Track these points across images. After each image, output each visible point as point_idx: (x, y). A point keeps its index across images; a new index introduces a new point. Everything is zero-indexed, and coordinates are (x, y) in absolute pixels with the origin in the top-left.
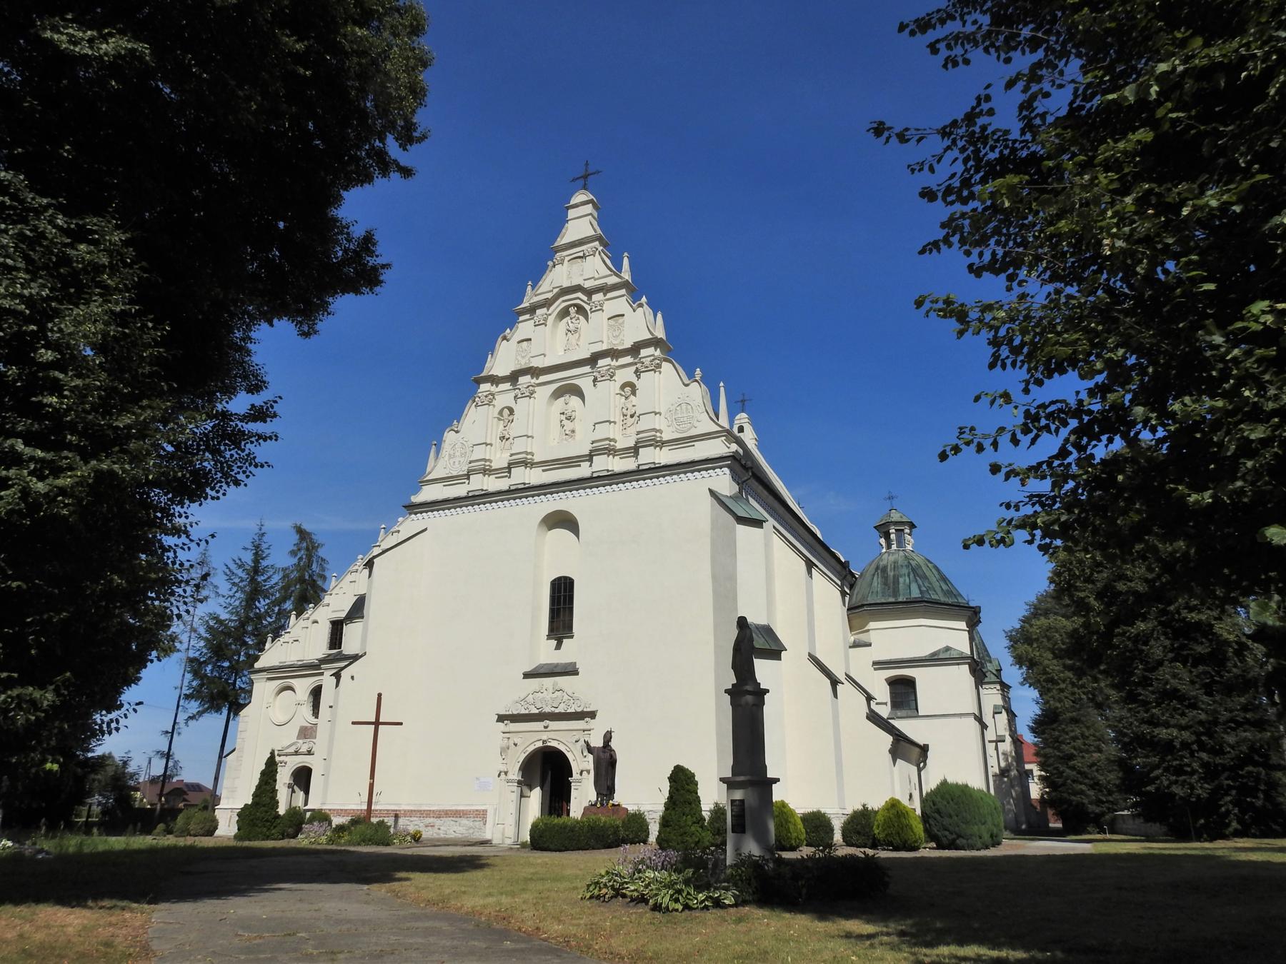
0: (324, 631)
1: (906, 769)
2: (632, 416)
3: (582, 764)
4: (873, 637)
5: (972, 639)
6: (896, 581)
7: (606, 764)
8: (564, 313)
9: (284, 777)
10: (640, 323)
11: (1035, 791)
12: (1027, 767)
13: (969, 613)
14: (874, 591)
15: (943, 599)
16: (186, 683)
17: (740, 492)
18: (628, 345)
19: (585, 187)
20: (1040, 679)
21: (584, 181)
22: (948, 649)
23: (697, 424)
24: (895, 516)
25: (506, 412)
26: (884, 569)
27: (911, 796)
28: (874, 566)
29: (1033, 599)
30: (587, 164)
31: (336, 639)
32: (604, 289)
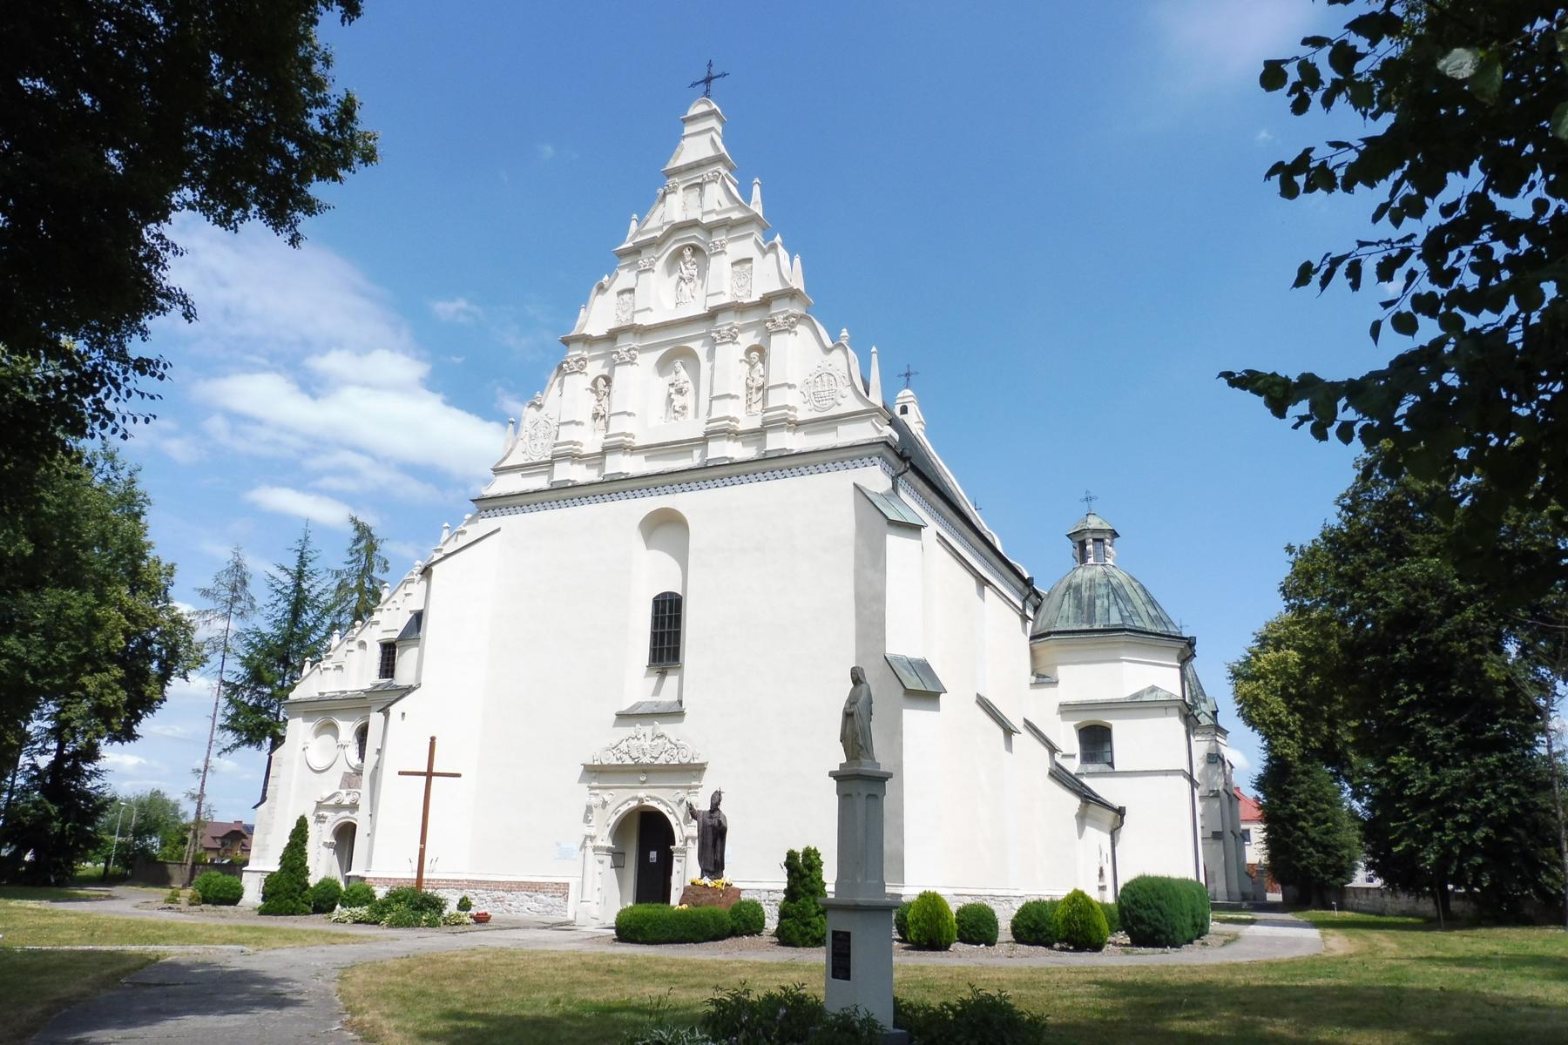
0: (375, 654)
1: (1097, 837)
2: (759, 389)
3: (685, 833)
4: (1063, 672)
5: (1183, 677)
6: (1092, 604)
7: (713, 836)
8: (678, 255)
9: (319, 839)
10: (776, 269)
11: (1255, 853)
12: (1244, 826)
13: (1182, 645)
14: (1063, 615)
15: (1150, 627)
16: (220, 711)
17: (895, 488)
18: (756, 298)
19: (707, 94)
20: (1270, 728)
22: (1153, 689)
23: (841, 401)
24: (1094, 523)
25: (602, 382)
26: (1077, 589)
27: (1101, 870)
28: (1065, 584)
29: (1260, 628)
30: (710, 65)
31: (388, 668)
32: (727, 225)
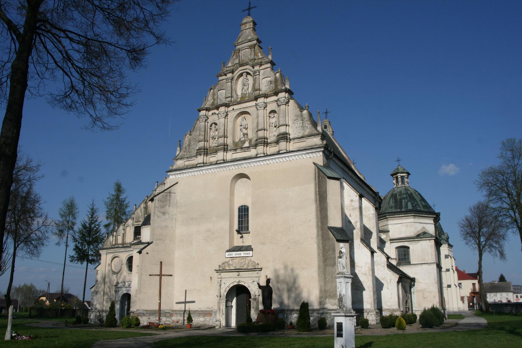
6: (401, 202)
21: (249, 11)
28: (390, 194)
30: (250, 3)
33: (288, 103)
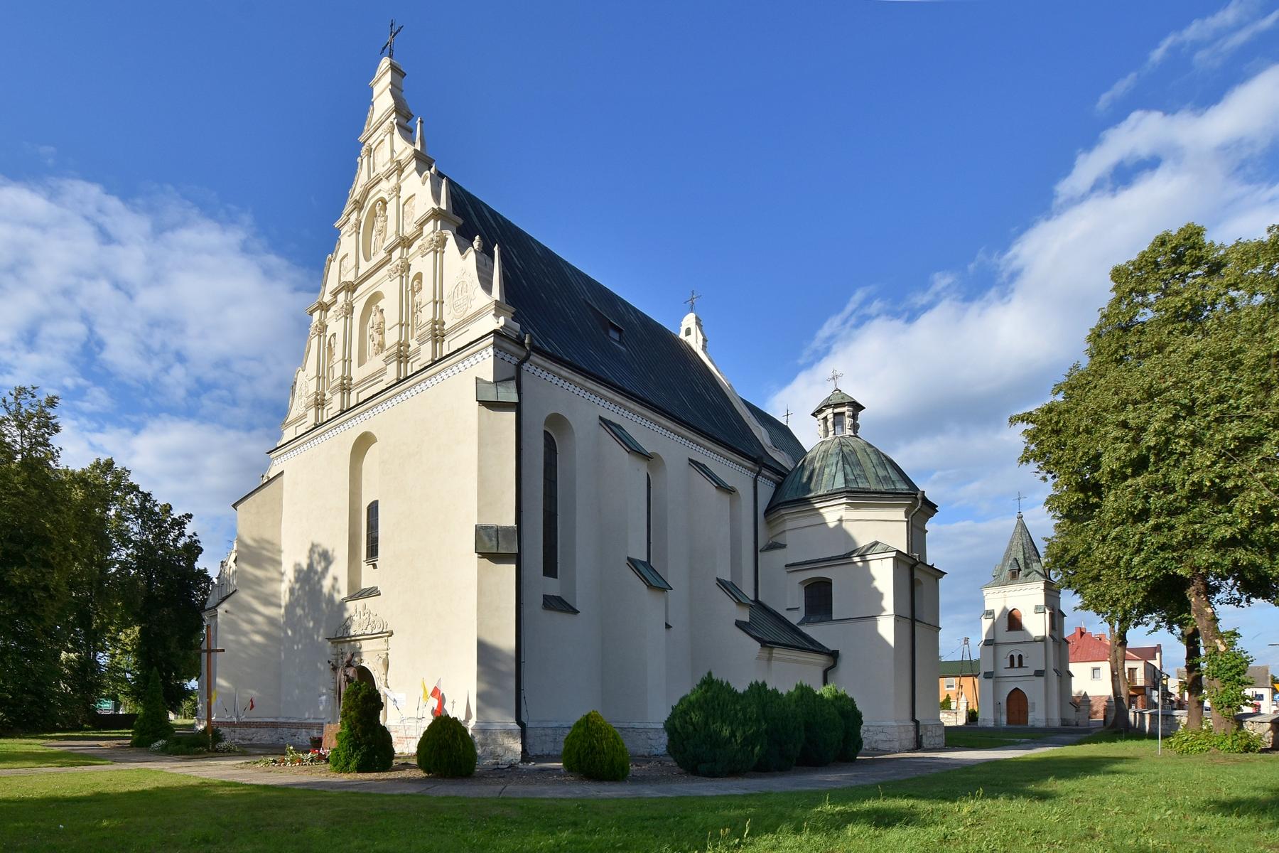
33: (442, 242)
